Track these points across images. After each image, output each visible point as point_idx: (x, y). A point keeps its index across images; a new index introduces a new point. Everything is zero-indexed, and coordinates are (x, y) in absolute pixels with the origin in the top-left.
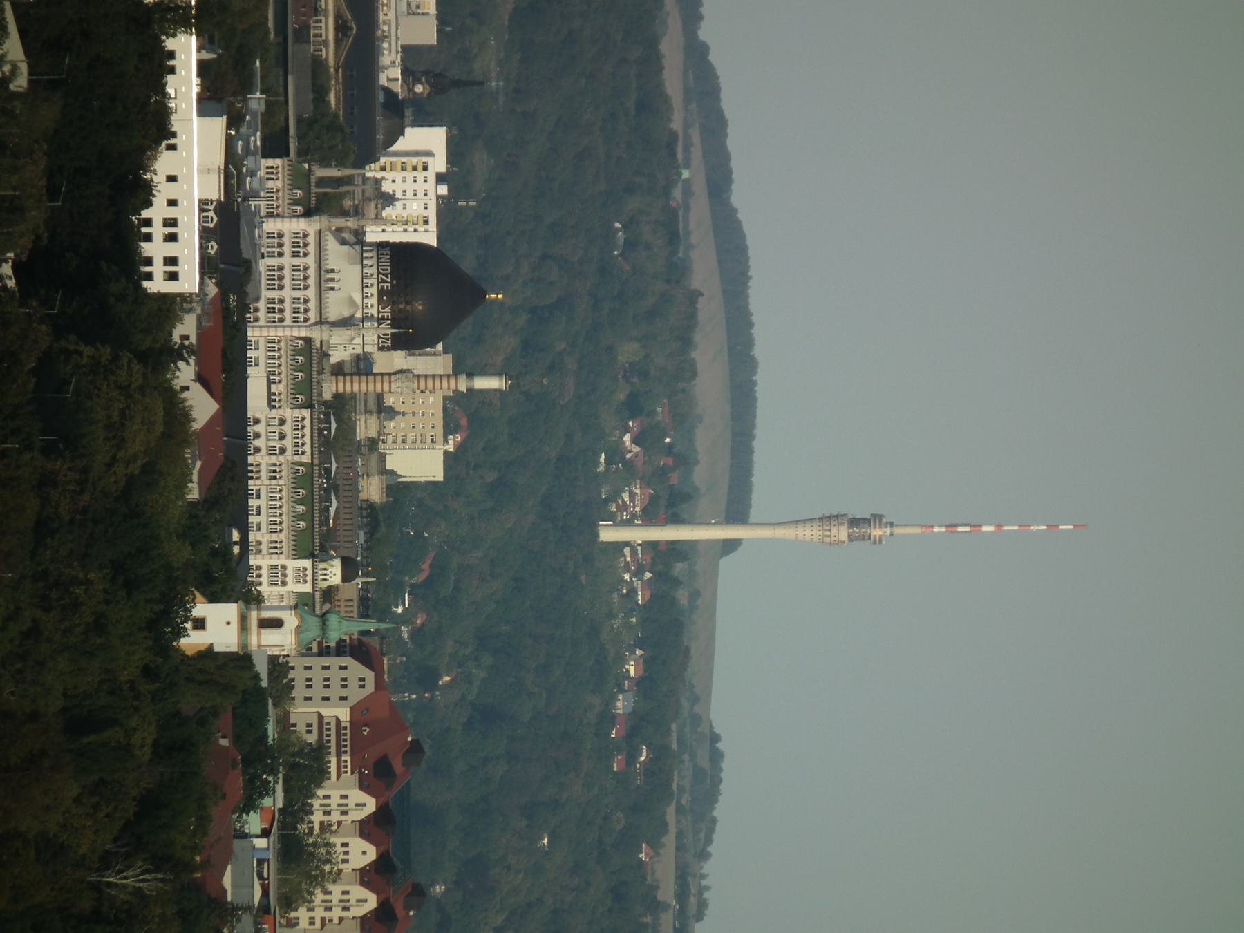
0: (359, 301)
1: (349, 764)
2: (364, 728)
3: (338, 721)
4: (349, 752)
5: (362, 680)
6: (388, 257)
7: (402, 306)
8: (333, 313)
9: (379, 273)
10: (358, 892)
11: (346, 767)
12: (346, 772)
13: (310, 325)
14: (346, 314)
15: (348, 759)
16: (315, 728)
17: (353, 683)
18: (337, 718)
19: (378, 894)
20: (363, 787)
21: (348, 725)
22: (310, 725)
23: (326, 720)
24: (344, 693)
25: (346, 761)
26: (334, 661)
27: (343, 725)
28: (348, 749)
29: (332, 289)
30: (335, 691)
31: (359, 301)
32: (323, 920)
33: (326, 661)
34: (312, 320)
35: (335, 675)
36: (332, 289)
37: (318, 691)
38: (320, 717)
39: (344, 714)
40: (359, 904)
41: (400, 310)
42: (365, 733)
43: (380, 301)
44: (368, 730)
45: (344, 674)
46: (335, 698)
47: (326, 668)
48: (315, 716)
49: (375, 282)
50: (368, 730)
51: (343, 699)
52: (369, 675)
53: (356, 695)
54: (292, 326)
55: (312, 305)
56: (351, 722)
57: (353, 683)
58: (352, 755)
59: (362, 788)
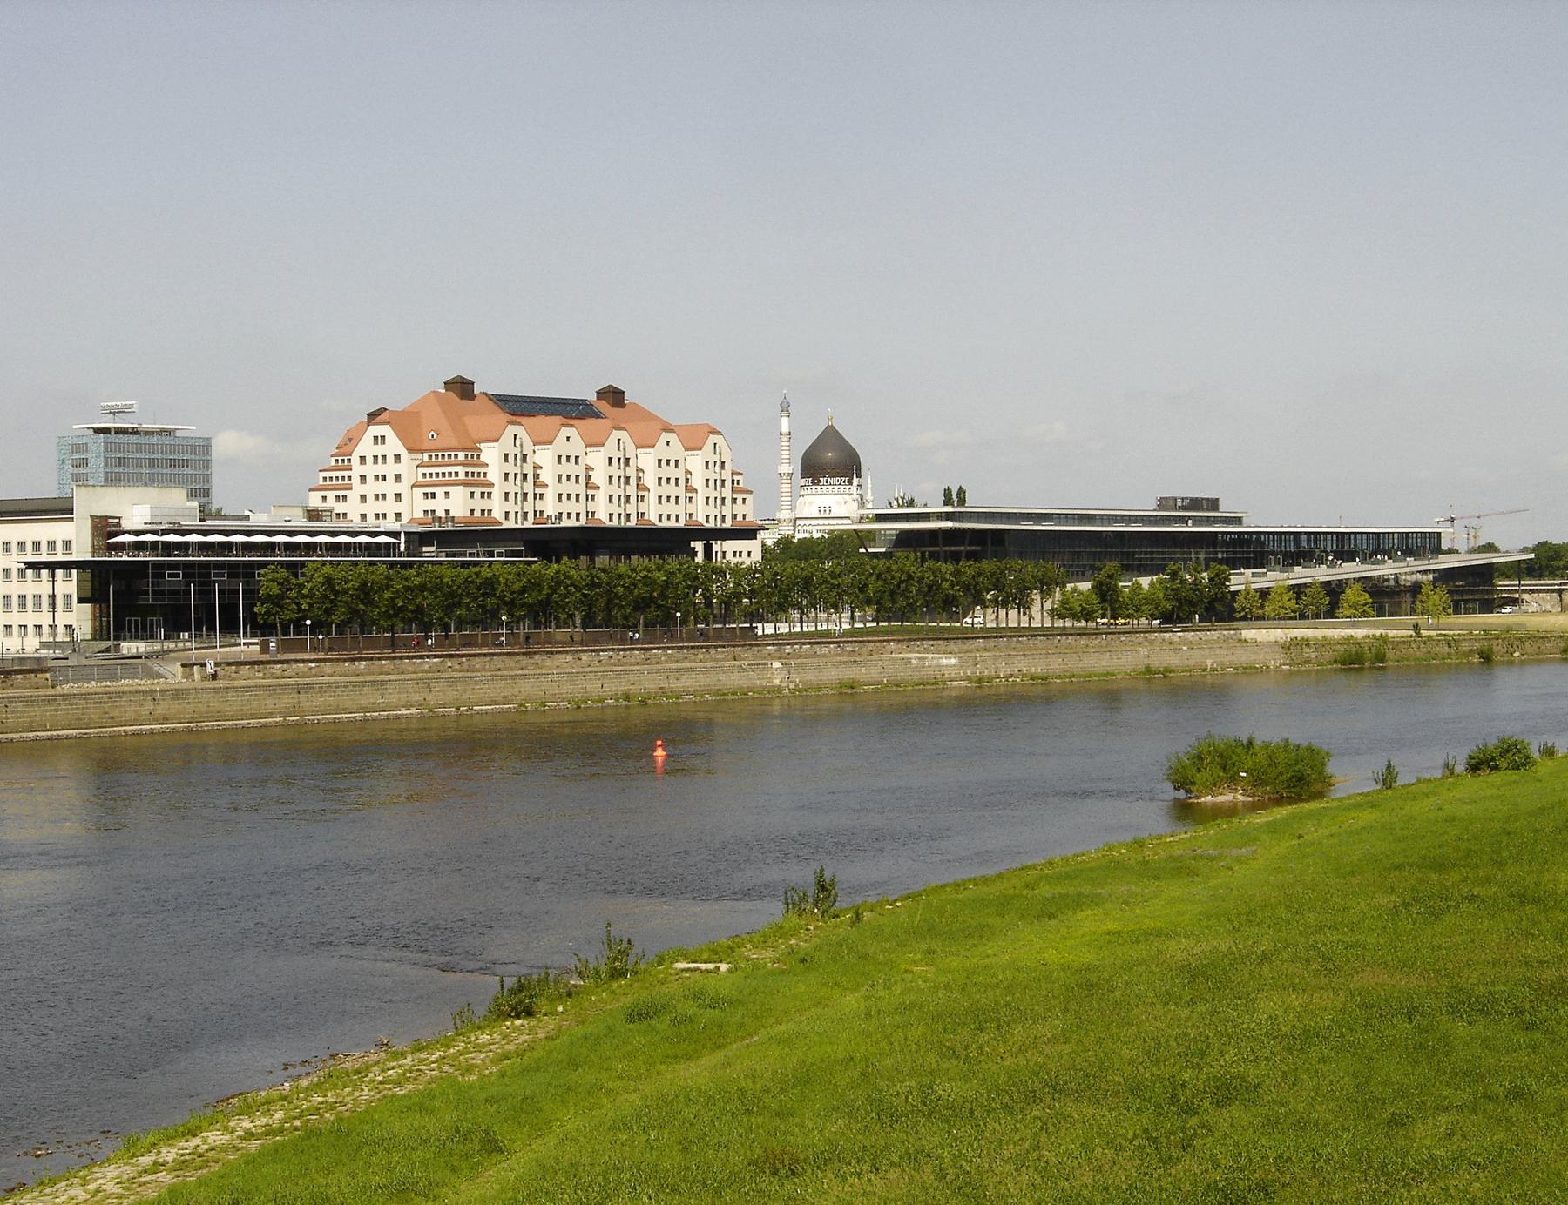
16: (429, 490)
17: (379, 450)
23: (420, 478)
24: (390, 459)
30: (390, 469)
35: (370, 470)
37: (389, 487)
44: (433, 433)
45: (370, 460)
50: (433, 433)
51: (397, 458)
53: (394, 445)
57: (379, 450)
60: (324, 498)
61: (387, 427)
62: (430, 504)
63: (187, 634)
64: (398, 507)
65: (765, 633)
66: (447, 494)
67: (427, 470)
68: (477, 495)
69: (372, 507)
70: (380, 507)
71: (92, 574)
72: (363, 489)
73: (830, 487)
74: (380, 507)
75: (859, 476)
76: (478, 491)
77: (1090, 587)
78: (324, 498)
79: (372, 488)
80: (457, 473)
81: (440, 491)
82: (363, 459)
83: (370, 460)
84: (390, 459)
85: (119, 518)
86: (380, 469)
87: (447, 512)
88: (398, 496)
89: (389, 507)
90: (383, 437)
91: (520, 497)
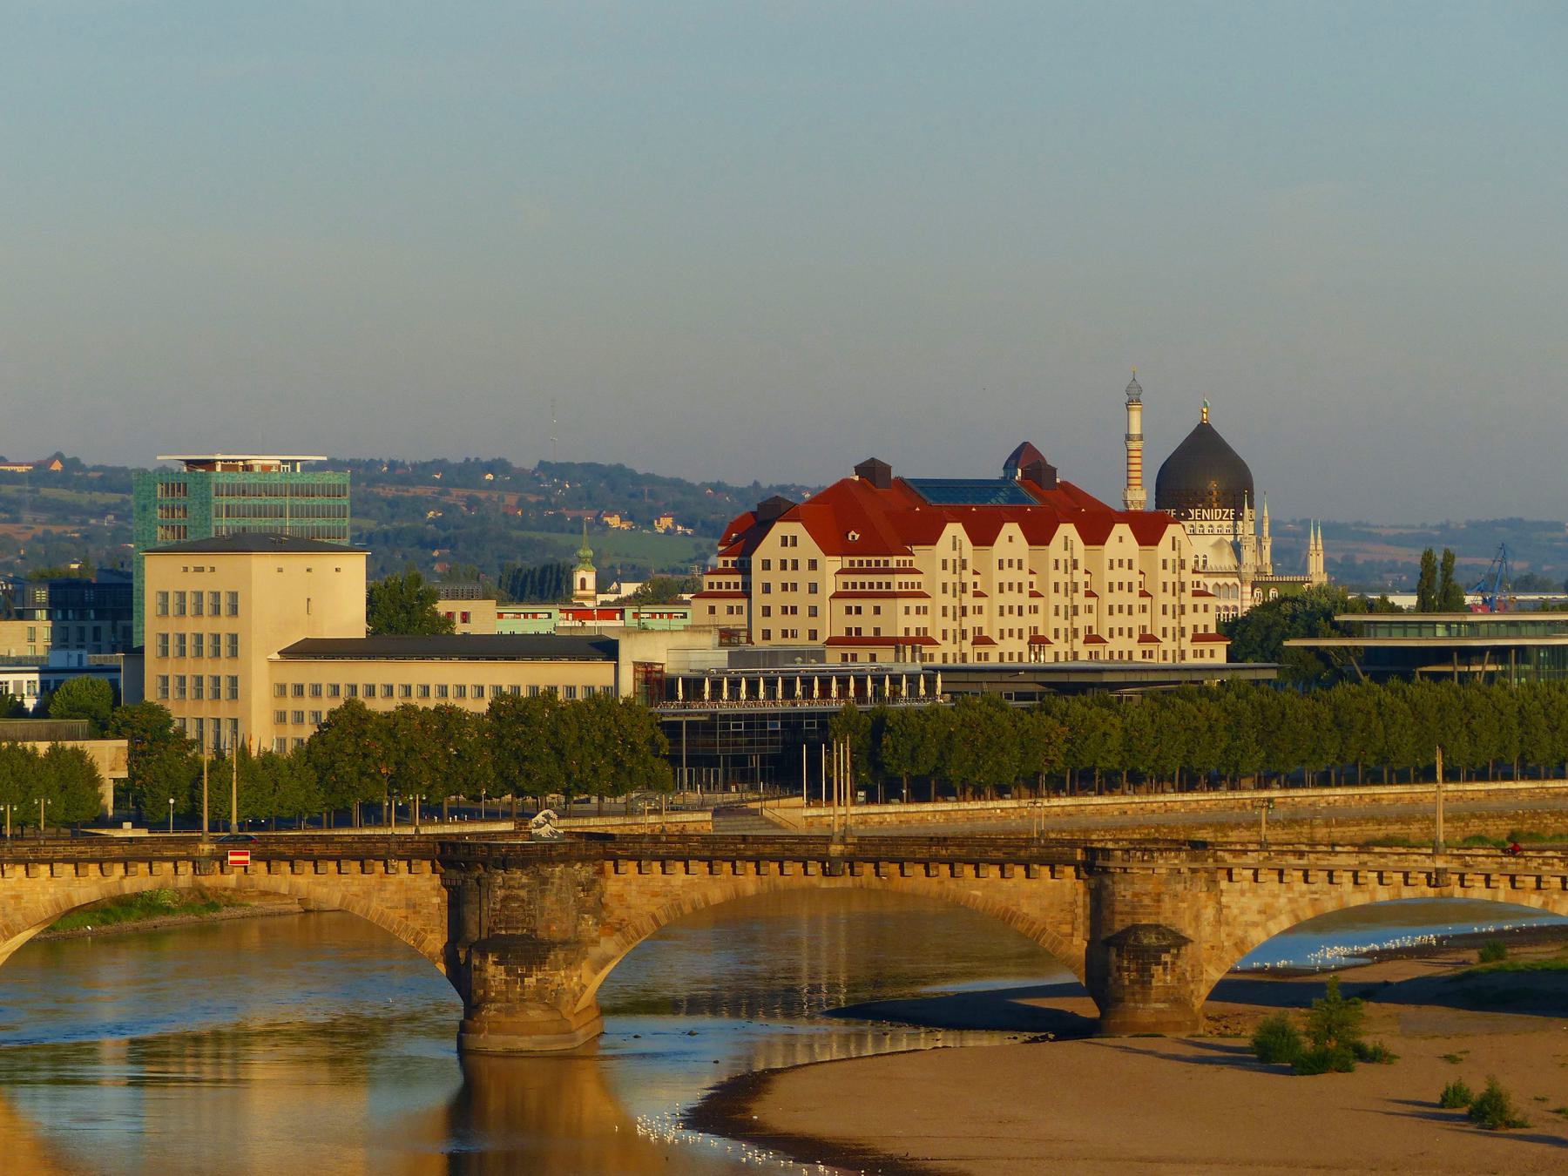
0: (1216, 538)
1: (902, 558)
2: (850, 538)
3: (842, 572)
4: (886, 558)
5: (784, 539)
6: (1204, 511)
7: (1214, 499)
8: (1228, 561)
9: (1221, 519)
10: (1056, 548)
11: (905, 562)
12: (911, 562)
13: (1242, 583)
14: (1227, 550)
15: (896, 558)
16: (854, 603)
17: (789, 553)
18: (838, 573)
19: (1114, 523)
20: (932, 540)
21: (847, 560)
22: (849, 610)
23: (841, 589)
24: (804, 565)
25: (898, 562)
26: (758, 577)
27: (847, 566)
28: (882, 559)
29: (1205, 562)
30: (803, 577)
31: (1216, 538)
32: (1196, 594)
33: (756, 589)
34: (1237, 581)
35: (776, 577)
36: (1205, 562)
37: (801, 599)
38: (837, 596)
39: (833, 564)
40: (1177, 547)
41: (1217, 501)
42: (857, 536)
43: (1186, 518)
44: (853, 533)
45: (775, 565)
46: (812, 576)
47: (767, 589)
48: (836, 602)
49: (1199, 523)
50: (853, 533)
51: (813, 565)
52: (780, 529)
53: (808, 547)
54: (1242, 600)
55: (1221, 581)
56: (842, 555)
57: (789, 553)
58: (891, 555)
59: (933, 542)
60: (712, 610)
61: (799, 525)
62: (854, 621)
63: (863, 799)
64: (813, 624)
65: (147, 865)
66: (877, 610)
67: (850, 579)
68: (913, 611)
69: (777, 623)
70: (789, 622)
71: (43, 658)
72: (766, 600)
73: (1206, 524)
74: (789, 622)
75: (1251, 507)
76: (913, 603)
77: (26, 706)
78: (712, 610)
79: (777, 599)
80: (888, 585)
81: (867, 605)
82: (766, 565)
83: (775, 565)
84: (804, 565)
85: (662, 664)
86: (789, 576)
87: (877, 630)
88: (813, 612)
89: (802, 623)
90: (794, 538)
91: (958, 612)
